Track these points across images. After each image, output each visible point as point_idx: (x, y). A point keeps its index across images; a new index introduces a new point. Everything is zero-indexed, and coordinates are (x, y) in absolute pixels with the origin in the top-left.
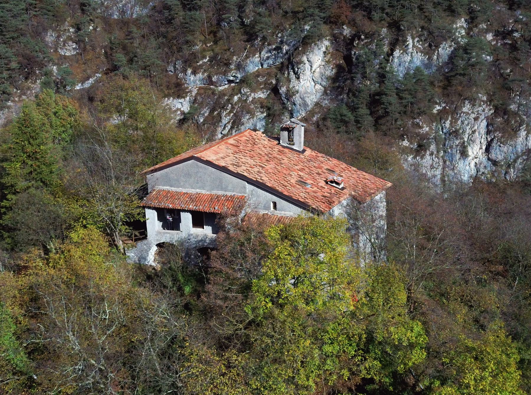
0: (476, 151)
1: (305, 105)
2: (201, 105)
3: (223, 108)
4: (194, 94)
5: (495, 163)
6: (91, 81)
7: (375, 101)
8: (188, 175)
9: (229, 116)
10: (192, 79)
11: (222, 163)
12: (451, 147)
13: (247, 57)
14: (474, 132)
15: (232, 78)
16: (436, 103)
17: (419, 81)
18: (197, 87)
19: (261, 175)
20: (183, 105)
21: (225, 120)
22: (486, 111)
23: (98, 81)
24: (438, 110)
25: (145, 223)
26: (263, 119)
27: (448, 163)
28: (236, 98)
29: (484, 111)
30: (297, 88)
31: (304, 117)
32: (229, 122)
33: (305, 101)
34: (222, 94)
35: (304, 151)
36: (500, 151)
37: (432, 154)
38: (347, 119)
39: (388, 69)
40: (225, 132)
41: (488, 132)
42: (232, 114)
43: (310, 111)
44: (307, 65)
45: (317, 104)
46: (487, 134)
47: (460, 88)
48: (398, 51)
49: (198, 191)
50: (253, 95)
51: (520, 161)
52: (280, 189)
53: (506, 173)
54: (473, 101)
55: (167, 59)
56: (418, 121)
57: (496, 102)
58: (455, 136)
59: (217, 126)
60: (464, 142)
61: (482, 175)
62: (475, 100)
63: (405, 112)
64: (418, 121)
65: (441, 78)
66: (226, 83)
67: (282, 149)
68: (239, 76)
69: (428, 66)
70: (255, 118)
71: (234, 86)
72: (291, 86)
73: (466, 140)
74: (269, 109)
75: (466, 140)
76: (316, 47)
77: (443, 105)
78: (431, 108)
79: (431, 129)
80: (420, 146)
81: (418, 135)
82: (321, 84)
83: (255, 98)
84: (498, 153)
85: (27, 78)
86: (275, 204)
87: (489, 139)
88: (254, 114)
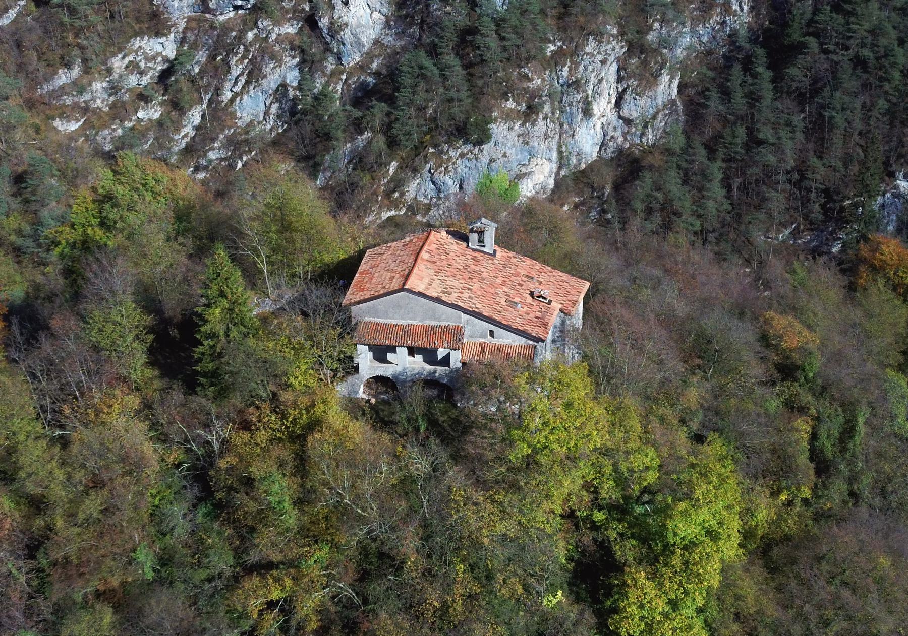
0: (603, 107)
1: (359, 44)
2: (194, 46)
3: (231, 50)
4: (181, 29)
5: (628, 122)
7: (467, 36)
8: (399, 307)
9: (242, 63)
10: (176, 5)
11: (435, 295)
12: (570, 105)
14: (600, 81)
16: (550, 42)
18: (184, 18)
19: (473, 301)
20: (166, 47)
21: (235, 71)
22: (617, 50)
24: (551, 52)
26: (296, 66)
27: (565, 127)
28: (250, 35)
29: (613, 50)
31: (358, 63)
32: (241, 74)
33: (359, 39)
34: (226, 28)
36: (635, 105)
37: (545, 118)
38: (429, 74)
40: (237, 89)
41: (619, 80)
42: (246, 61)
43: (367, 54)
45: (376, 42)
46: (618, 83)
47: (582, 19)
49: (410, 322)
50: (276, 29)
51: (660, 116)
52: (496, 317)
54: (599, 35)
56: (526, 71)
57: (630, 36)
58: (575, 89)
60: (587, 97)
61: (610, 140)
62: (602, 34)
66: (231, 9)
70: (283, 66)
71: (245, 15)
72: (336, 17)
73: (590, 92)
74: (303, 52)
75: (590, 92)
77: (559, 44)
78: (541, 50)
79: (543, 80)
80: (529, 107)
81: (526, 90)
82: (380, 12)
83: (280, 35)
84: (633, 109)
87: (620, 89)
88: (281, 60)
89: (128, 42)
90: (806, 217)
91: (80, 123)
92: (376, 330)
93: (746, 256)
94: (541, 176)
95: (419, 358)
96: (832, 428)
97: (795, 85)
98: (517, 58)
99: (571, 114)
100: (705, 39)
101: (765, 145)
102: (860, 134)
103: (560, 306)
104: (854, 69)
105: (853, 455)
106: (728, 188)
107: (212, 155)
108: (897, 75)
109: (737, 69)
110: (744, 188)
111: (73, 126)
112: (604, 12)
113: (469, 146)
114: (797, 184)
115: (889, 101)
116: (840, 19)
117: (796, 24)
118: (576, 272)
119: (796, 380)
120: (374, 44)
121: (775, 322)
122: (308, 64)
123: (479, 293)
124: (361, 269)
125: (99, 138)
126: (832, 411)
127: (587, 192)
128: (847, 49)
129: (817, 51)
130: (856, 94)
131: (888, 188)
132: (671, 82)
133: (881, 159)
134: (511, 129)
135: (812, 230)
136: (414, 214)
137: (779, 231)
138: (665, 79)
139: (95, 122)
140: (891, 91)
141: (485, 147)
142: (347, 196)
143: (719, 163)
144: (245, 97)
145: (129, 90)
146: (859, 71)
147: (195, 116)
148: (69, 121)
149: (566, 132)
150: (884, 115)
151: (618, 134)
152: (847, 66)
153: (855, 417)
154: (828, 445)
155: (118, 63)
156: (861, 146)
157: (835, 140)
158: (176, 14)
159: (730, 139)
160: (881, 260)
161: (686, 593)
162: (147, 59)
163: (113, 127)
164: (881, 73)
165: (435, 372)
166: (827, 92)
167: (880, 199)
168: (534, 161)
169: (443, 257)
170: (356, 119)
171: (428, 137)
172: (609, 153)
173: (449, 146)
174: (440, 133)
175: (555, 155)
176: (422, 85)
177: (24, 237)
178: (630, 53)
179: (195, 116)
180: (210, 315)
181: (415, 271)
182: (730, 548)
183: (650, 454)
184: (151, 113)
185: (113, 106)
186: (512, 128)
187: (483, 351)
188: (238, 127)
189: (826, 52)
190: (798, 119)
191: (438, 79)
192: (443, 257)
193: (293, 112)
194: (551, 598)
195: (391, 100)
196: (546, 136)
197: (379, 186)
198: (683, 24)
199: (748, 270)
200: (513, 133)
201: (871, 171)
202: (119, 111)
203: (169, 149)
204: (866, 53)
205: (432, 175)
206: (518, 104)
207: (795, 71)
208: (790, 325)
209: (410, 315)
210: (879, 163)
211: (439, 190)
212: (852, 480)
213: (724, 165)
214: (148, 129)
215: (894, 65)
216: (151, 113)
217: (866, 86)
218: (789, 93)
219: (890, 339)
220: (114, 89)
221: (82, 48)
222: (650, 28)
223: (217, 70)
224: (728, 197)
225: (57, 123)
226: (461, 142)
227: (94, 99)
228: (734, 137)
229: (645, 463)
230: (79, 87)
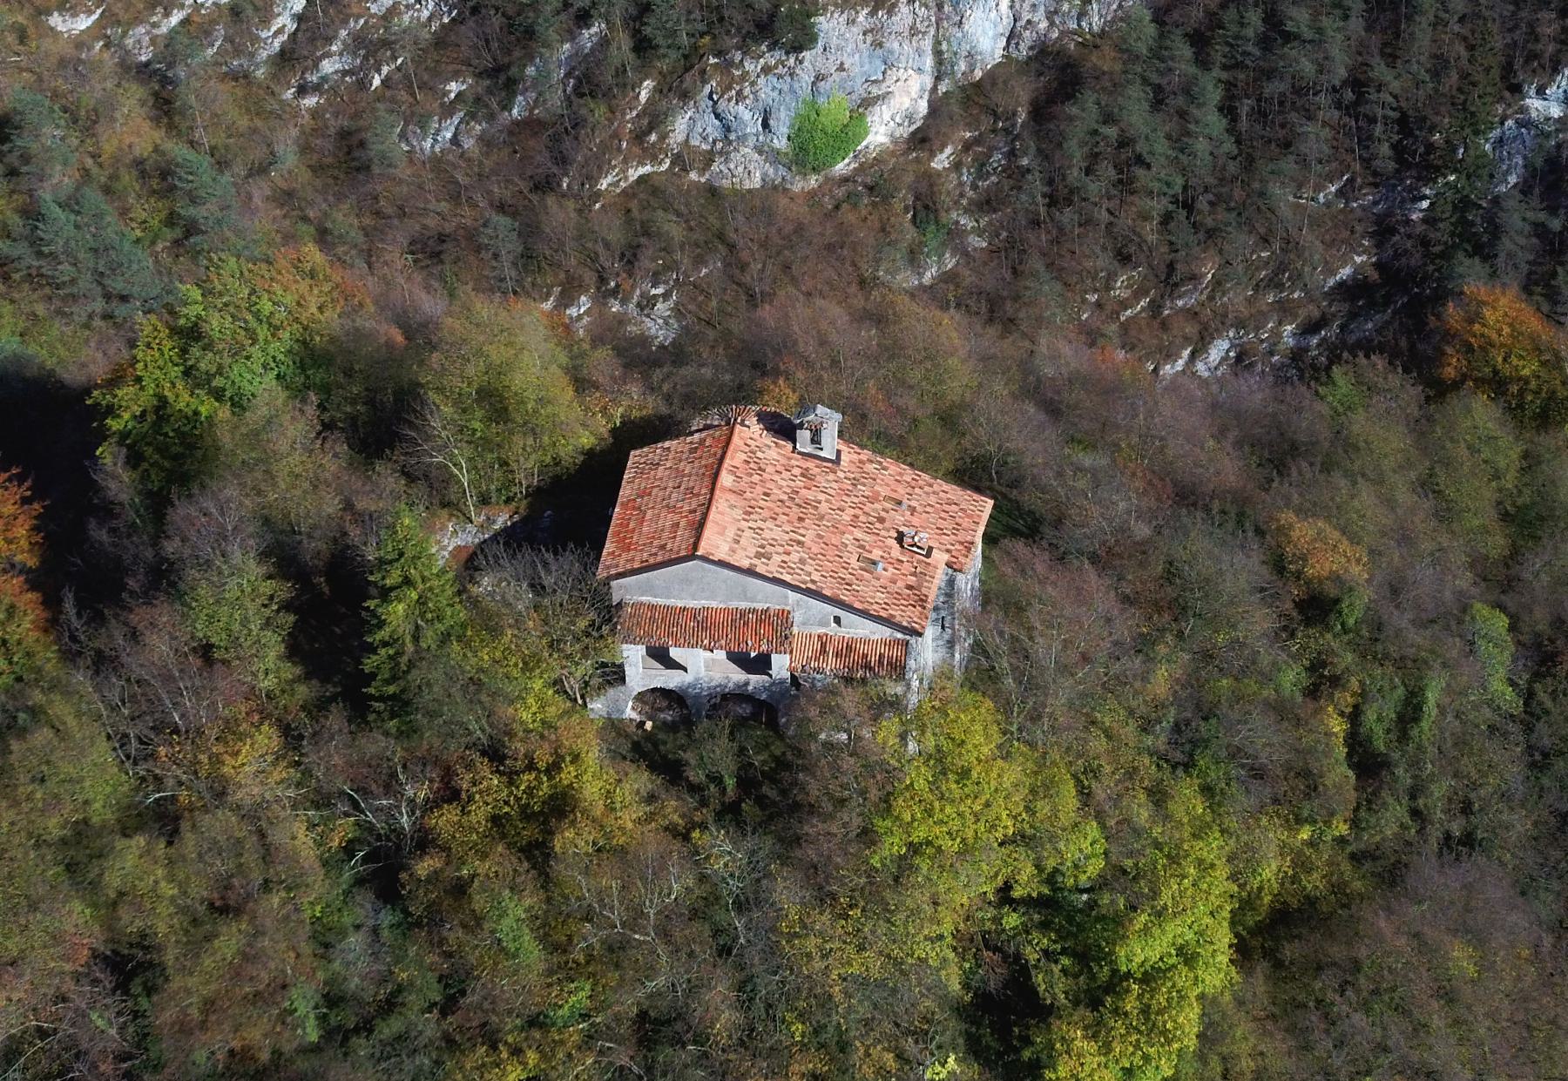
8: (687, 581)
11: (745, 563)
19: (808, 568)
25: (621, 666)
27: (946, 8)
35: (839, 452)
53: (1082, 15)
61: (1025, 28)
90: (1366, 162)
91: (95, 17)
93: (1262, 231)
94: (907, 96)
96: (1378, 719)
101: (1296, 44)
103: (946, 557)
105: (1420, 748)
107: (328, 67)
110: (1260, 114)
111: (83, 23)
113: (778, 54)
114: (1350, 109)
118: (970, 475)
119: (1328, 628)
121: (1295, 534)
123: (815, 549)
124: (625, 492)
125: (129, 42)
127: (986, 122)
131: (1509, 112)
133: (1495, 61)
134: (851, 22)
135: (1376, 185)
136: (685, 170)
137: (1318, 188)
139: (121, 13)
141: (806, 54)
142: (568, 143)
143: (1217, 72)
148: (75, 15)
149: (948, 18)
154: (1379, 731)
157: (1418, 34)
159: (1234, 28)
161: (1146, 1058)
163: (155, 19)
165: (747, 684)
168: (893, 75)
169: (756, 478)
171: (707, 39)
172: (1024, 51)
173: (744, 53)
174: (728, 32)
175: (929, 62)
177: (15, 240)
180: (389, 614)
181: (712, 515)
182: (1217, 971)
186: (854, 21)
187: (823, 651)
188: (373, 16)
192: (756, 478)
194: (938, 1068)
196: (914, 31)
197: (623, 122)
200: (854, 29)
203: (252, 55)
205: (715, 103)
210: (1496, 73)
213: (1224, 75)
225: (55, 20)
226: (764, 48)
228: (1242, 25)
229: (1083, 852)
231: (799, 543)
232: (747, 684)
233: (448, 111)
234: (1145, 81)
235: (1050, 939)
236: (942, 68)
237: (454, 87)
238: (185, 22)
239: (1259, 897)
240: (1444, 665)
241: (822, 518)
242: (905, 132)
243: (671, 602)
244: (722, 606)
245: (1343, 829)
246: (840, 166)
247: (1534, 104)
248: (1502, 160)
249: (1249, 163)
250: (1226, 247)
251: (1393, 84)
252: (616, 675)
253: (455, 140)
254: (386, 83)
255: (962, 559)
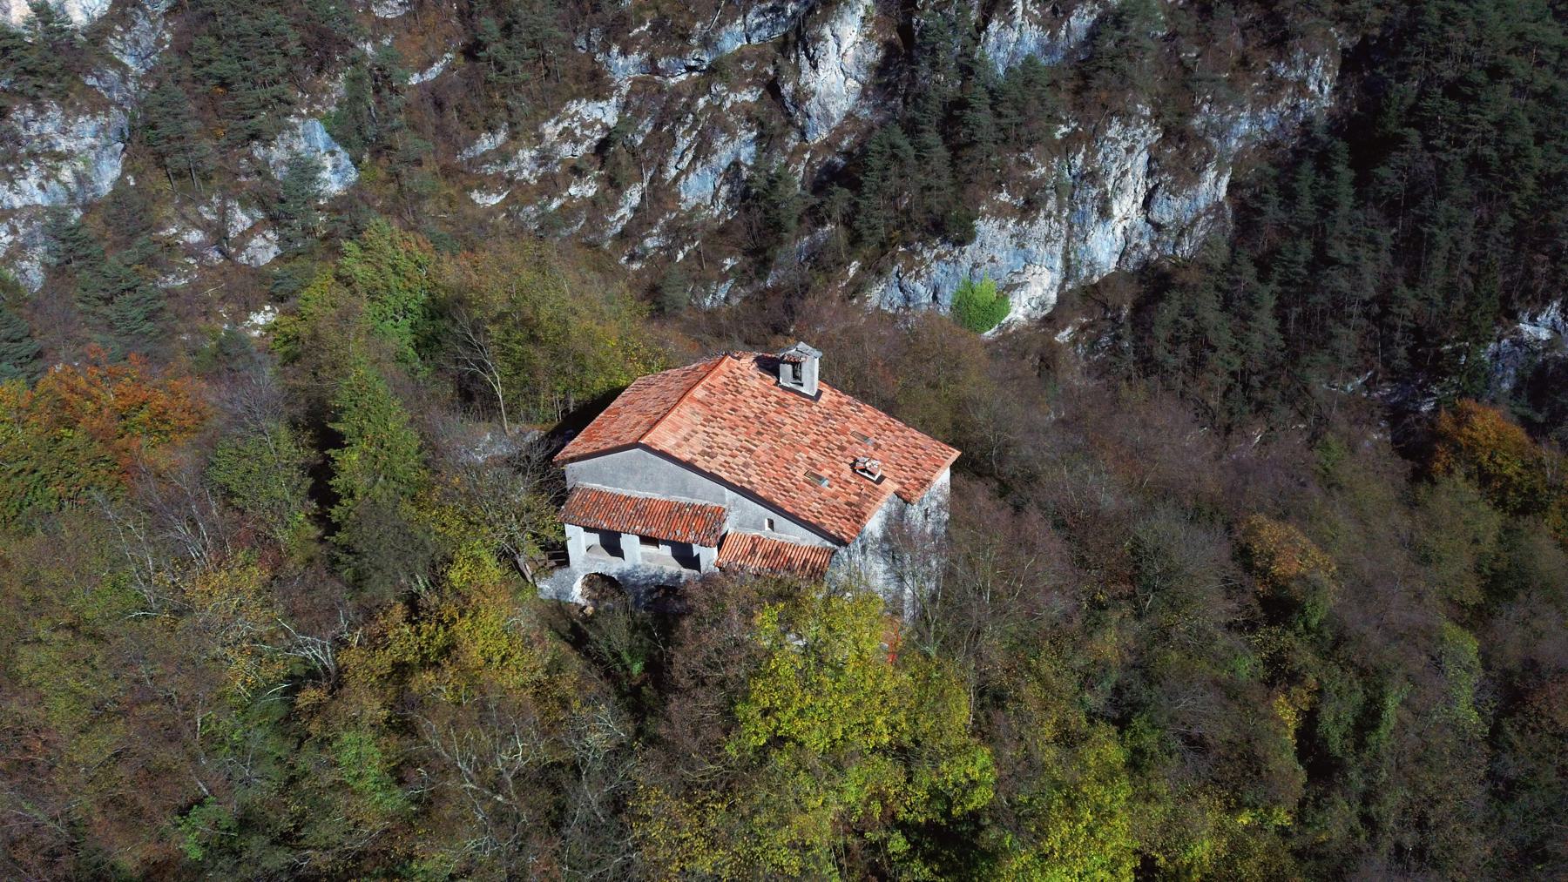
0: (1126, 207)
1: (827, 117)
2: (638, 113)
3: (679, 120)
4: (624, 92)
5: (1158, 227)
6: (437, 68)
7: (955, 111)
8: (631, 470)
11: (686, 457)
12: (1083, 201)
13: (721, 24)
14: (1124, 174)
15: (693, 63)
16: (1061, 122)
17: (1028, 83)
19: (749, 471)
20: (606, 113)
21: (682, 144)
23: (449, 68)
25: (564, 547)
28: (701, 102)
29: (1144, 135)
30: (813, 85)
32: (689, 147)
34: (677, 92)
35: (819, 393)
38: (901, 155)
39: (977, 56)
41: (1150, 173)
44: (832, 44)
45: (849, 116)
47: (1104, 95)
48: (995, 22)
49: (649, 495)
52: (779, 500)
53: (1177, 244)
54: (1126, 117)
55: (573, 25)
59: (669, 155)
60: (1106, 193)
62: (1130, 115)
63: (1005, 141)
64: (1027, 155)
65: (1071, 73)
67: (782, 395)
68: (707, 59)
69: (1048, 50)
72: (802, 83)
73: (1110, 187)
74: (761, 125)
75: (1110, 187)
76: (847, 10)
78: (1049, 131)
79: (1050, 169)
80: (1027, 202)
81: (1027, 180)
85: (319, 71)
86: (771, 524)
89: (563, 105)
90: (1386, 363)
92: (596, 503)
93: (1301, 408)
94: (1038, 289)
95: (665, 551)
97: (1385, 190)
98: (1014, 139)
99: (1084, 214)
100: (1269, 127)
102: (1472, 258)
103: (897, 487)
104: (1468, 173)
106: (1284, 320)
107: (649, 243)
108: (1530, 182)
109: (1307, 167)
110: (1304, 320)
111: (494, 200)
112: (1133, 86)
113: (948, 246)
115: (1514, 217)
116: (1455, 105)
117: (1392, 112)
119: (1291, 627)
120: (846, 118)
121: (1265, 533)
122: (766, 140)
123: (763, 458)
126: (1345, 684)
128: (1462, 145)
129: (1418, 147)
130: (1470, 206)
132: (1218, 179)
133: (1498, 292)
135: (1394, 381)
137: (1347, 380)
138: (1211, 175)
140: (1520, 204)
141: (968, 248)
143: (1273, 286)
144: (692, 176)
145: (562, 161)
146: (1475, 176)
147: (634, 196)
148: (489, 194)
150: (1506, 235)
151: (1145, 242)
152: (1460, 167)
153: (1382, 695)
155: (550, 130)
156: (1472, 275)
157: (1435, 265)
158: (620, 75)
159: (1289, 255)
160: (1470, 437)
162: (584, 125)
164: (1507, 179)
165: (679, 576)
166: (1427, 201)
167: (1492, 346)
168: (1031, 269)
170: (813, 207)
172: (1131, 265)
175: (1058, 264)
176: (894, 169)
178: (1167, 138)
179: (634, 196)
183: (980, 761)
184: (583, 189)
185: (541, 179)
187: (753, 552)
189: (1432, 149)
190: (1385, 237)
191: (912, 161)
193: (745, 195)
195: (856, 186)
198: (1242, 109)
199: (1302, 426)
200: (1004, 233)
201: (1483, 308)
202: (550, 185)
203: (602, 232)
204: (1487, 151)
206: (1014, 197)
207: (1386, 173)
208: (1289, 539)
209: (651, 485)
211: (908, 299)
212: (1367, 798)
213: (1279, 289)
214: (579, 208)
215: (1526, 169)
216: (583, 189)
217: (1485, 196)
218: (1377, 201)
219: (1467, 561)
220: (544, 159)
221: (509, 110)
222: (1198, 109)
223: (662, 143)
224: (1282, 329)
225: (475, 195)
227: (520, 170)
228: (1297, 253)
230: (504, 155)
231: (750, 451)
232: (679, 576)
233: (724, 278)
234: (1218, 288)
235: (932, 870)
236: (1069, 269)
237: (729, 262)
238: (562, 206)
239: (1188, 873)
240: (1408, 677)
241: (782, 436)
242: (1040, 314)
243: (618, 491)
244: (664, 498)
245: (1283, 818)
246: (988, 333)
247: (1527, 328)
248: (1497, 370)
249: (1294, 357)
250: (1273, 417)
251: (1409, 304)
252: (559, 555)
253: (727, 299)
254: (686, 257)
255: (913, 492)
